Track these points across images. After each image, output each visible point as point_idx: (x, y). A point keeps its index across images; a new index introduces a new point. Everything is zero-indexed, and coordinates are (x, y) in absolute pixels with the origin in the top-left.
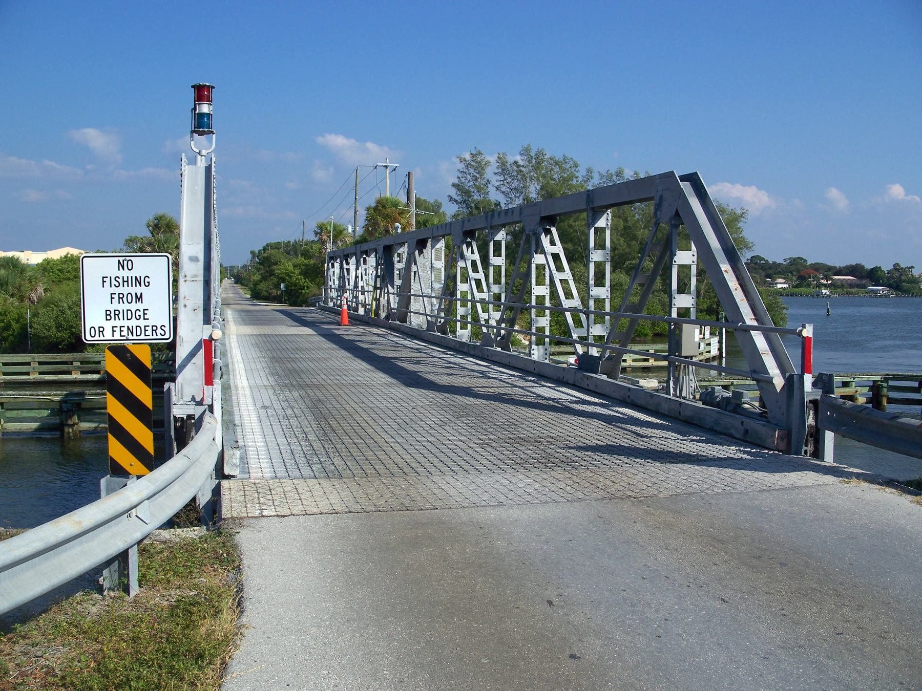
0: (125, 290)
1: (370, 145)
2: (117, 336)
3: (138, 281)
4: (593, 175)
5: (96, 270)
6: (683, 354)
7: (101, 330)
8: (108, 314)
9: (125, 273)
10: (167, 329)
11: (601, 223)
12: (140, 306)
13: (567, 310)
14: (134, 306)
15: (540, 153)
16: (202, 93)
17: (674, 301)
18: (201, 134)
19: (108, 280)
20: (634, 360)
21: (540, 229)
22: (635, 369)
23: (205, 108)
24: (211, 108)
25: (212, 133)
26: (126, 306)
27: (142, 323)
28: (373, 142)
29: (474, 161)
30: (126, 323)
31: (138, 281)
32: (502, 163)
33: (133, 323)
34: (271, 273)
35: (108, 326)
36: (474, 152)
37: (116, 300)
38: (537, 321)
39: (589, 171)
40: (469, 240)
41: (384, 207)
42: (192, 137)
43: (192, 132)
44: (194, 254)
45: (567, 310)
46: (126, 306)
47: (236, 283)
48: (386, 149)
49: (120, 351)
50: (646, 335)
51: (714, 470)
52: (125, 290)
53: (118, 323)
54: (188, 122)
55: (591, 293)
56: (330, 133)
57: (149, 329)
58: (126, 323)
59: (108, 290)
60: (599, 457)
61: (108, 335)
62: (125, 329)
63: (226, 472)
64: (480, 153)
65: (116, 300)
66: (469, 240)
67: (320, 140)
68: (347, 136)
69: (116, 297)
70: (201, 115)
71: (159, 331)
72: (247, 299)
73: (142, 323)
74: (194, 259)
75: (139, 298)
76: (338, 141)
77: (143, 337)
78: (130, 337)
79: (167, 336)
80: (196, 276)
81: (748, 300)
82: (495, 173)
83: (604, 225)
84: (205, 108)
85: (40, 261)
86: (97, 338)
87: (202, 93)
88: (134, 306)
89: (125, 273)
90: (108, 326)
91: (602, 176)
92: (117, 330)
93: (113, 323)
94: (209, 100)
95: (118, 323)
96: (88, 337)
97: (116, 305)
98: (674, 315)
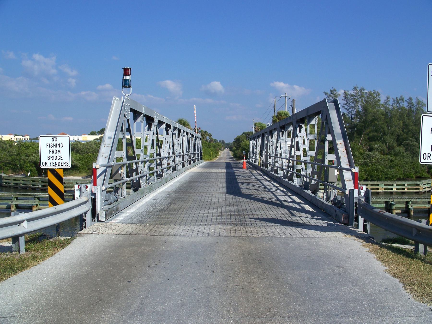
0: (54, 149)
1: (296, 87)
2: (52, 166)
3: (59, 145)
4: (390, 99)
5: (45, 142)
6: (329, 181)
7: (46, 163)
8: (48, 157)
9: (54, 142)
10: (69, 163)
11: (313, 122)
12: (59, 154)
13: (303, 162)
14: (57, 155)
15: (362, 89)
16: (127, 71)
17: (326, 157)
18: (127, 88)
19: (48, 145)
20: (397, 189)
21: (297, 125)
22: (397, 193)
23: (128, 77)
24: (130, 77)
25: (130, 87)
26: (55, 155)
27: (60, 161)
28: (296, 85)
29: (332, 94)
30: (55, 161)
31: (59, 145)
32: (346, 94)
33: (57, 161)
34: (239, 146)
35: (48, 162)
36: (332, 90)
37: (51, 152)
38: (297, 167)
39: (388, 98)
40: (283, 130)
41: (281, 115)
42: (123, 89)
43: (123, 87)
44: (110, 136)
45: (303, 162)
46: (55, 155)
47: (230, 151)
48: (303, 88)
49: (53, 171)
50: (412, 177)
51: (306, 231)
52: (54, 149)
53: (52, 161)
54: (121, 83)
55: (308, 154)
56: (276, 81)
57: (63, 163)
58: (55, 161)
59: (49, 148)
60: (263, 223)
61: (49, 165)
62: (54, 163)
63: (100, 220)
64: (335, 90)
65: (51, 152)
66: (283, 130)
67: (272, 84)
68: (284, 83)
69: (51, 151)
70: (126, 81)
71: (66, 164)
72: (231, 158)
73: (60, 161)
74: (110, 138)
75: (59, 152)
76: (281, 85)
77: (60, 166)
78: (56, 166)
79: (69, 166)
80: (109, 144)
81: (348, 156)
82: (343, 100)
83: (314, 123)
84: (128, 77)
85: (92, 140)
86: (45, 166)
87: (127, 71)
88: (57, 155)
89: (54, 142)
90: (48, 162)
91: (394, 100)
92: (52, 163)
93: (50, 160)
94: (129, 74)
95: (52, 161)
96: (42, 166)
97: (51, 154)
98: (326, 163)
